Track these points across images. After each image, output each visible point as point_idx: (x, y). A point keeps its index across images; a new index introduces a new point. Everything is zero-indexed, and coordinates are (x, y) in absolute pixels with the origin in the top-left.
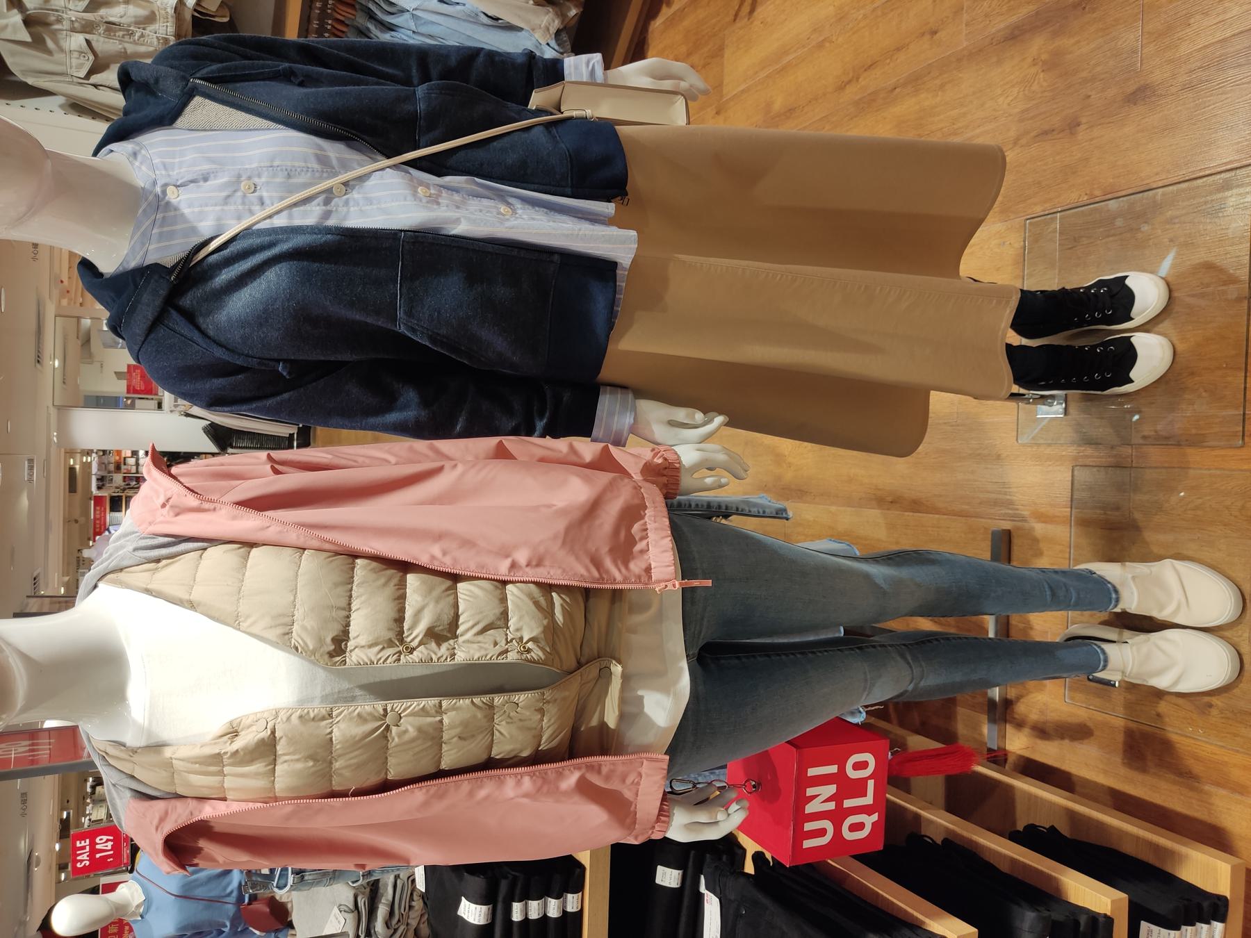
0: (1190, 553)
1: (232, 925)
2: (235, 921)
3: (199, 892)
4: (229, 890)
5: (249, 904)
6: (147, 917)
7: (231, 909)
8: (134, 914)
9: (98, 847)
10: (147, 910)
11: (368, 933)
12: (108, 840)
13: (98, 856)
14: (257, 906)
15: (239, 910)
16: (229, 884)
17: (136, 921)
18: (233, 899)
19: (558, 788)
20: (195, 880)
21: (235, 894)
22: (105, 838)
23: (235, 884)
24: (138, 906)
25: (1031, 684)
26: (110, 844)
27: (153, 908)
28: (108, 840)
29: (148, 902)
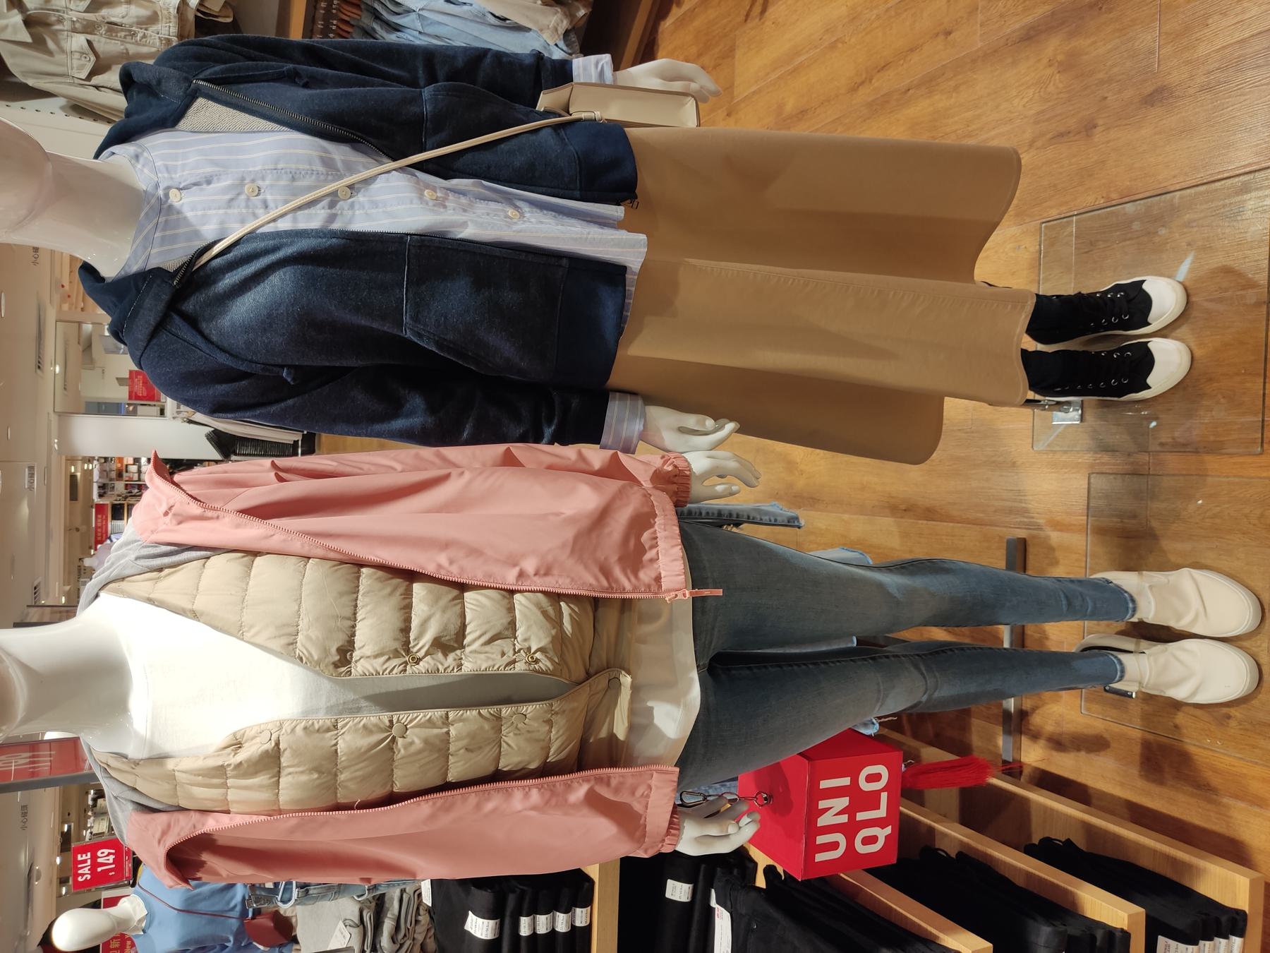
0: (1208, 562)
1: (235, 940)
2: (238, 935)
3: (202, 907)
4: (232, 905)
5: (253, 918)
6: (149, 932)
7: (234, 924)
8: (136, 928)
9: (99, 860)
10: (149, 925)
11: (374, 948)
12: (109, 854)
13: (99, 869)
14: (261, 920)
15: (242, 924)
16: (232, 898)
17: (138, 936)
18: (236, 913)
19: (566, 801)
20: (198, 894)
21: (238, 908)
22: (107, 851)
23: (238, 898)
24: (140, 921)
25: (1047, 695)
26: (111, 857)
27: (156, 923)
28: (109, 854)
29: (150, 917)
